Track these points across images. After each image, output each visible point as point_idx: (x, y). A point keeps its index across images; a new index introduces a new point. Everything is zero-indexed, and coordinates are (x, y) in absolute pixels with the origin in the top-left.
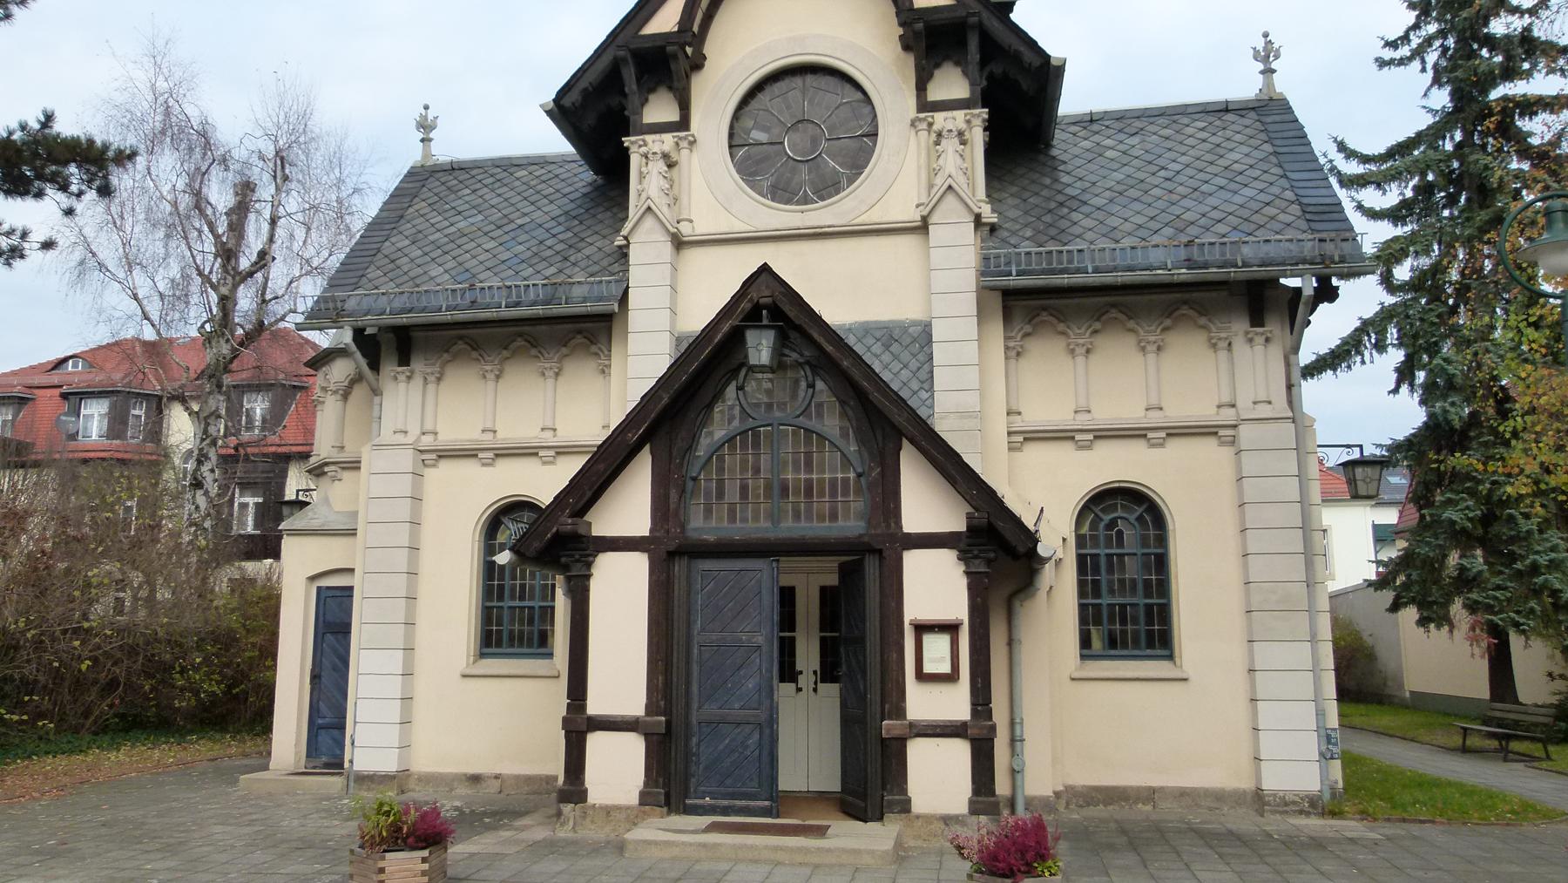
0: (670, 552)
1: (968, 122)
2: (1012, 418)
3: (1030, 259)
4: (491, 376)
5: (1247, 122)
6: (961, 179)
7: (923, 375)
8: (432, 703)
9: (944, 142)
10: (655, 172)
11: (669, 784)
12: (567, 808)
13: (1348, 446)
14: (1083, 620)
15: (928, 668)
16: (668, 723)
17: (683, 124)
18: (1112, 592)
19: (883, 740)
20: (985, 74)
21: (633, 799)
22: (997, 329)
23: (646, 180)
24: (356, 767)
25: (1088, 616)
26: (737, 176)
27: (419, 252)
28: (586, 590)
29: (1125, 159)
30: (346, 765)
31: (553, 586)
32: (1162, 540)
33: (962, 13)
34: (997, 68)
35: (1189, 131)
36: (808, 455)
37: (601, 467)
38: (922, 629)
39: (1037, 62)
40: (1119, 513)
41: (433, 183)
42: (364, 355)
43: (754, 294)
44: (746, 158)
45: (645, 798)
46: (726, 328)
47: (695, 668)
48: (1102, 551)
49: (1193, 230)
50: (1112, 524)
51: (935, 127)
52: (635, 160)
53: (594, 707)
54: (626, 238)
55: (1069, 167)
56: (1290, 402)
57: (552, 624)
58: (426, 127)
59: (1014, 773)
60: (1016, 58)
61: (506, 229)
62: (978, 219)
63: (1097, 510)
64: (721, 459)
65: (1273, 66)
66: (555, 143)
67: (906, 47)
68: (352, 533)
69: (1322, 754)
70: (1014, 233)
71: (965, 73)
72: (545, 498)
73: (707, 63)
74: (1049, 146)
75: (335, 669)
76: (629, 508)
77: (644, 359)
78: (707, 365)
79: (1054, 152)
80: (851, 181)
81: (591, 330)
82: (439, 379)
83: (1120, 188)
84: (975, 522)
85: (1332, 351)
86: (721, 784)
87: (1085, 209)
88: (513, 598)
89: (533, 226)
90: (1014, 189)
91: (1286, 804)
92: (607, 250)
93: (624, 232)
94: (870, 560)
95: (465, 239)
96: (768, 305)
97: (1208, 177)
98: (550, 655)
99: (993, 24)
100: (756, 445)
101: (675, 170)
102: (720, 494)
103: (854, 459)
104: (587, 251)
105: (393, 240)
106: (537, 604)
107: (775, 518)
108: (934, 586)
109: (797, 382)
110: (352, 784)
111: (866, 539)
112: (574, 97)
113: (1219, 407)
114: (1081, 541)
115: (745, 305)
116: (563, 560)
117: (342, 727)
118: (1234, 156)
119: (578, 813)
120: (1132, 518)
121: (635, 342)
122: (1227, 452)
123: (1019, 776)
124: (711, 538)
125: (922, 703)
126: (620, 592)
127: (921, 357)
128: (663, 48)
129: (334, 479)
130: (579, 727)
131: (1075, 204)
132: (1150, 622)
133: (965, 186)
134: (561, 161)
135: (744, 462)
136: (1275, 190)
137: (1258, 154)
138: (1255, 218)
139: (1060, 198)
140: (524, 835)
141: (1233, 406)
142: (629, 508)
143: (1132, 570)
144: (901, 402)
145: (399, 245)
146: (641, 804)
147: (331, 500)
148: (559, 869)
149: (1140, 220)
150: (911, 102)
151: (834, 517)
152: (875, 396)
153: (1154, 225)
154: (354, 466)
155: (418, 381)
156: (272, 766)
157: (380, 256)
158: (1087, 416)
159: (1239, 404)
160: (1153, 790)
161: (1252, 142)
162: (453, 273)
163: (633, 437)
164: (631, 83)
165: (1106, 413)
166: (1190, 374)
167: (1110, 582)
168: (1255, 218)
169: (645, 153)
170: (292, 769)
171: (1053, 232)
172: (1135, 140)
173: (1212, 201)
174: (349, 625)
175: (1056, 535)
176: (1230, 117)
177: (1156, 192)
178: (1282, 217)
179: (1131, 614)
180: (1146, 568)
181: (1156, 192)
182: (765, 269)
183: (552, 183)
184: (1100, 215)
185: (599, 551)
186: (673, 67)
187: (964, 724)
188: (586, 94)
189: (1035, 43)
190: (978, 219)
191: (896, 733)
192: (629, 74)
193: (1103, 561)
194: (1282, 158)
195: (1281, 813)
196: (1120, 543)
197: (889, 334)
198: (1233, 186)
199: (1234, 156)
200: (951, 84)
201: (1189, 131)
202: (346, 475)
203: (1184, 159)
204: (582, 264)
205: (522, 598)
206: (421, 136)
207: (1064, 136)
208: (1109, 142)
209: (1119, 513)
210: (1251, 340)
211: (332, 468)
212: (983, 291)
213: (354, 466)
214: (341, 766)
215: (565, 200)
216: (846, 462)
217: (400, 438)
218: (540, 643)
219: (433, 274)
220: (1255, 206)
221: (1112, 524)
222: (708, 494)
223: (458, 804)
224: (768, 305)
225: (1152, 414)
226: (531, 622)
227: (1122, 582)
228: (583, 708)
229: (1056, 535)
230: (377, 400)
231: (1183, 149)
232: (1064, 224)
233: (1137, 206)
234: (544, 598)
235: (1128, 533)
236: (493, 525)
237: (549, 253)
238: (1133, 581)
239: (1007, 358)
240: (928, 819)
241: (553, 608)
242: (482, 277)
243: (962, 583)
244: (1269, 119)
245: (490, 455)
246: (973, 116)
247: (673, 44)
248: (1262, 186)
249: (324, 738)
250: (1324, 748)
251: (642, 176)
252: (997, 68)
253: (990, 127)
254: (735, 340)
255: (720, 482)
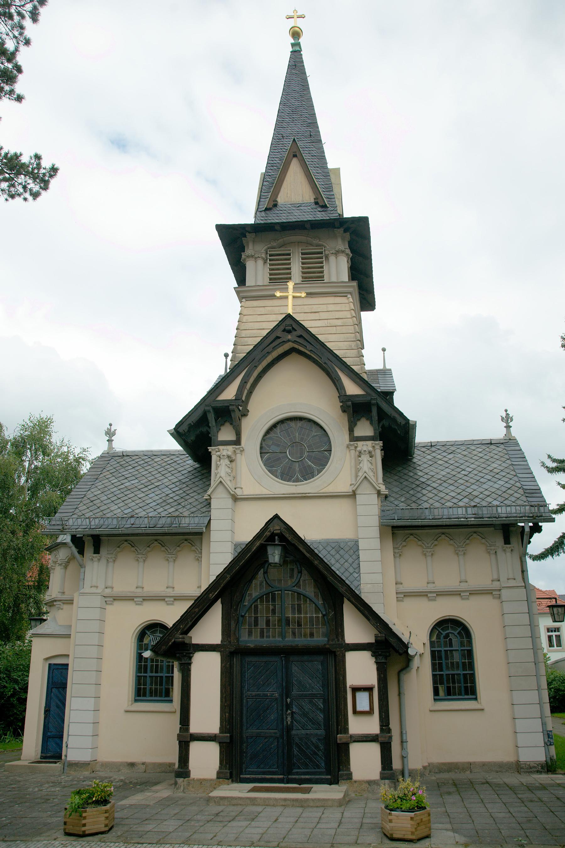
0: (233, 654)
1: (374, 447)
2: (398, 586)
3: (402, 511)
4: (141, 560)
5: (500, 449)
6: (371, 474)
7: (355, 565)
8: (109, 724)
9: (362, 456)
10: (224, 464)
11: (233, 767)
12: (180, 781)
13: (550, 598)
14: (435, 682)
15: (359, 709)
16: (231, 737)
17: (237, 442)
18: (447, 668)
19: (338, 745)
20: (381, 425)
21: (214, 776)
22: (389, 544)
23: (220, 469)
24: (68, 759)
25: (437, 680)
26: (264, 467)
27: (106, 498)
28: (189, 670)
29: (447, 465)
30: (63, 757)
31: (173, 666)
32: (470, 643)
33: (369, 398)
34: (386, 423)
35: (475, 453)
36: (299, 606)
37: (197, 610)
38: (355, 690)
39: (403, 422)
40: (450, 631)
41: (113, 462)
42: (76, 547)
43: (271, 528)
44: (269, 459)
45: (220, 775)
46: (258, 544)
47: (245, 709)
48: (443, 649)
49: (477, 500)
50: (447, 636)
51: (358, 449)
52: (214, 458)
53: (194, 728)
54: (209, 496)
55: (421, 468)
56: (523, 579)
57: (172, 685)
58: (110, 434)
59: (403, 758)
60: (394, 420)
61: (150, 487)
62: (379, 493)
63: (439, 629)
64: (256, 607)
65: (510, 424)
66: (174, 446)
67: (344, 411)
68: (68, 636)
69: (545, 743)
70: (396, 499)
71: (371, 423)
72: (170, 622)
73: (249, 413)
74: (410, 460)
75: (58, 706)
76: (210, 629)
77: (219, 557)
78: (249, 561)
79: (415, 460)
80: (319, 472)
81: (190, 539)
82: (114, 561)
83: (443, 479)
84: (379, 638)
85: (551, 547)
86: (258, 767)
87: (429, 488)
88: (152, 672)
89: (163, 486)
90: (396, 478)
91: (531, 768)
92: (201, 500)
93: (209, 493)
94: (333, 654)
95: (129, 492)
96: (277, 534)
97: (483, 475)
98: (171, 701)
99: (384, 406)
100: (274, 600)
101: (234, 464)
102: (256, 624)
103: (321, 607)
104: (190, 501)
105: (92, 490)
106: (164, 674)
107: (282, 635)
108: (360, 669)
109: (292, 570)
110: (66, 768)
111: (328, 646)
112: (185, 427)
113: (492, 581)
114: (432, 644)
115: (267, 534)
116: (178, 655)
117: (61, 737)
118: (494, 465)
119: (185, 783)
120: (456, 633)
121: (214, 547)
122: (496, 602)
123: (405, 760)
124: (252, 646)
125: (357, 726)
126: (207, 671)
127: (354, 557)
128: (229, 406)
129: (59, 609)
130: (186, 739)
131: (424, 486)
132: (466, 682)
133: (372, 477)
134: (179, 454)
135: (268, 608)
136: (512, 482)
137: (505, 465)
138: (504, 495)
139: (417, 483)
140: (158, 795)
141: (499, 580)
142: (210, 629)
143: (457, 657)
144: (342, 581)
145: (96, 493)
146: (218, 778)
147: (54, 621)
148: (175, 812)
149: (453, 494)
150: (347, 437)
151: (312, 635)
152: (330, 578)
153: (460, 497)
154: (70, 602)
155: (104, 561)
156: (22, 757)
157: (85, 498)
158: (434, 585)
159: (501, 580)
160: (470, 764)
161: (502, 459)
162: (123, 509)
163: (212, 596)
164: (212, 423)
165: (442, 584)
166: (477, 566)
167: (447, 664)
168: (504, 495)
169: (219, 455)
170: (34, 760)
171: (414, 499)
172: (451, 456)
173: (485, 486)
174: (66, 684)
175: (419, 642)
176: (492, 447)
177: (461, 481)
178: (516, 495)
179: (456, 679)
180: (463, 656)
181: (461, 481)
182: (276, 517)
183: (173, 465)
184: (435, 491)
185: (195, 651)
186: (233, 416)
187: (377, 735)
188: (191, 427)
189: (402, 414)
190: (379, 493)
191: (344, 741)
192: (211, 417)
193: (443, 653)
194: (515, 467)
195: (529, 772)
196: (451, 645)
197: (338, 546)
198: (494, 479)
199: (494, 465)
200: (365, 428)
201: (475, 453)
202: (65, 607)
203: (472, 466)
204: (188, 507)
205: (156, 672)
206: (108, 438)
207: (419, 453)
208: (439, 457)
209: (450, 631)
210: (505, 550)
211: (58, 603)
212: (383, 527)
213: (70, 602)
214: (60, 757)
215: (179, 474)
216: (317, 609)
217: (94, 590)
218: (166, 695)
219: (112, 509)
220: (504, 489)
221: (447, 636)
222: (250, 625)
223: (122, 778)
224: (277, 534)
225: (462, 584)
226: (161, 684)
227: (452, 663)
228: (187, 729)
229: (419, 642)
230: (82, 570)
231: (472, 461)
232: (419, 495)
233: (452, 488)
234: (168, 673)
235: (454, 640)
236: (142, 635)
237: (171, 500)
238: (458, 663)
239: (395, 557)
240: (360, 782)
241: (173, 677)
242: (137, 511)
243: (374, 667)
244: (509, 449)
245: (141, 599)
246: (376, 444)
247: (233, 405)
248: (507, 480)
249: (52, 744)
250: (546, 740)
251: (217, 467)
252: (386, 423)
253: (384, 449)
254: (262, 550)
255: (256, 619)
